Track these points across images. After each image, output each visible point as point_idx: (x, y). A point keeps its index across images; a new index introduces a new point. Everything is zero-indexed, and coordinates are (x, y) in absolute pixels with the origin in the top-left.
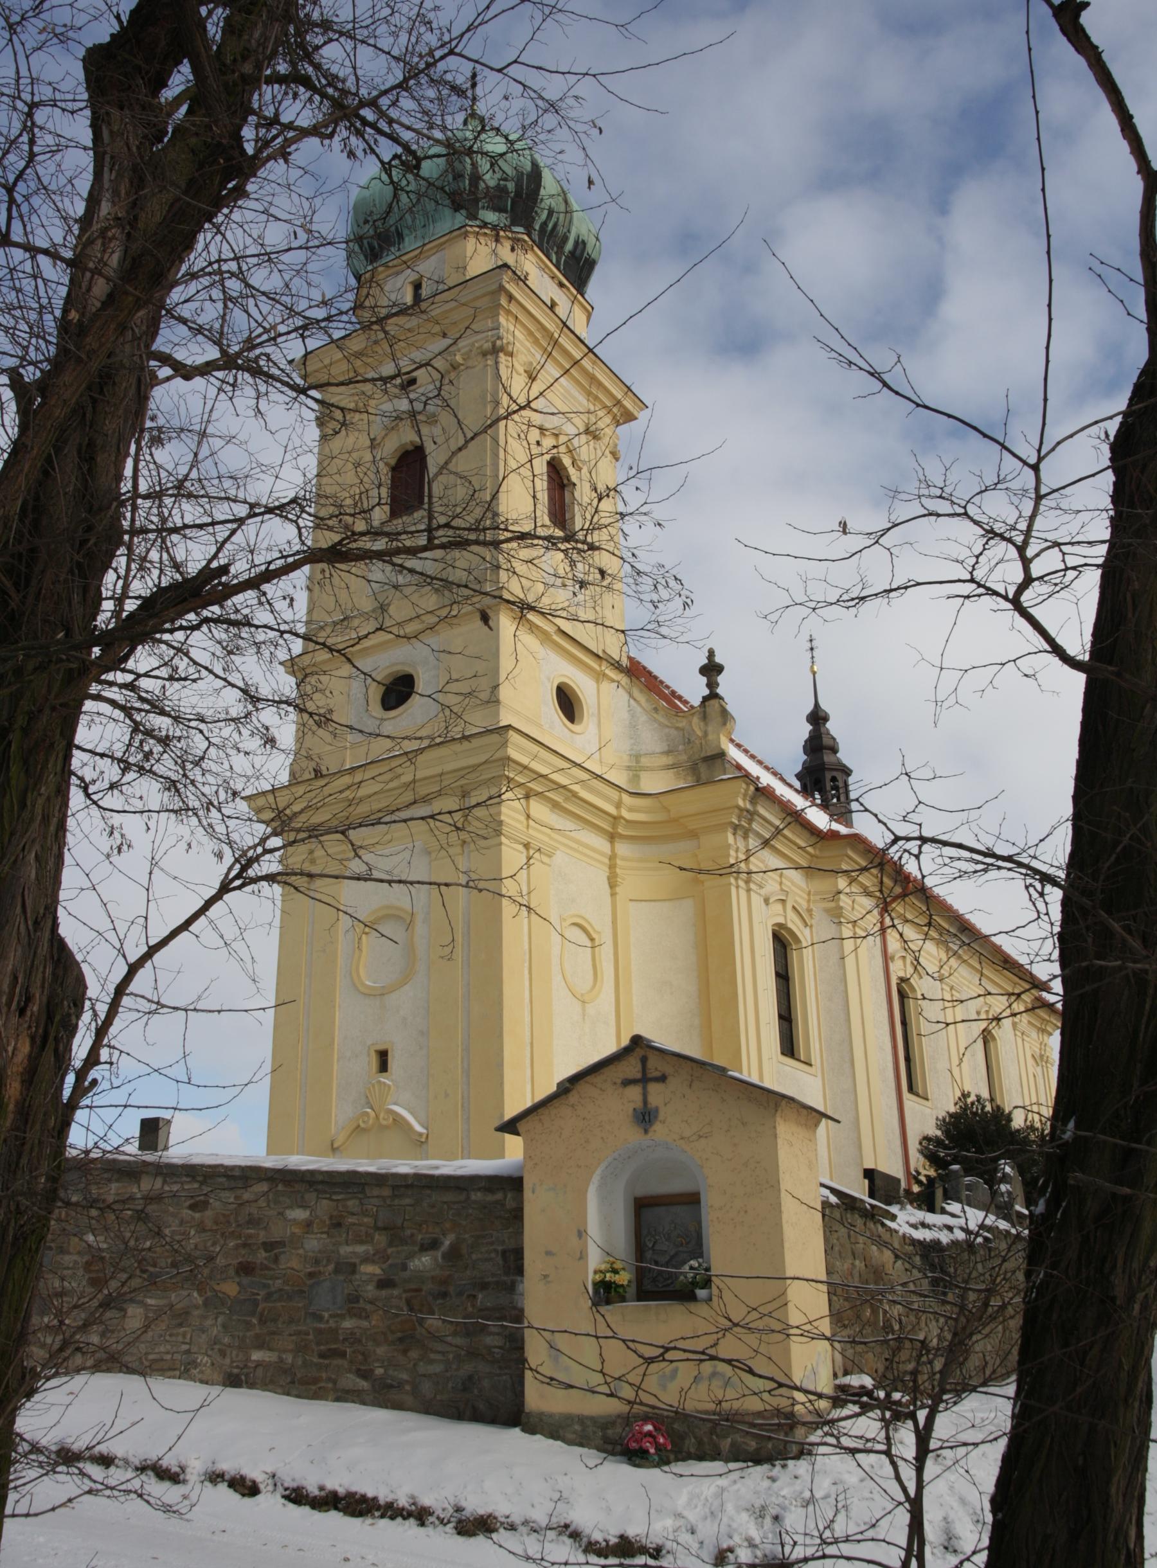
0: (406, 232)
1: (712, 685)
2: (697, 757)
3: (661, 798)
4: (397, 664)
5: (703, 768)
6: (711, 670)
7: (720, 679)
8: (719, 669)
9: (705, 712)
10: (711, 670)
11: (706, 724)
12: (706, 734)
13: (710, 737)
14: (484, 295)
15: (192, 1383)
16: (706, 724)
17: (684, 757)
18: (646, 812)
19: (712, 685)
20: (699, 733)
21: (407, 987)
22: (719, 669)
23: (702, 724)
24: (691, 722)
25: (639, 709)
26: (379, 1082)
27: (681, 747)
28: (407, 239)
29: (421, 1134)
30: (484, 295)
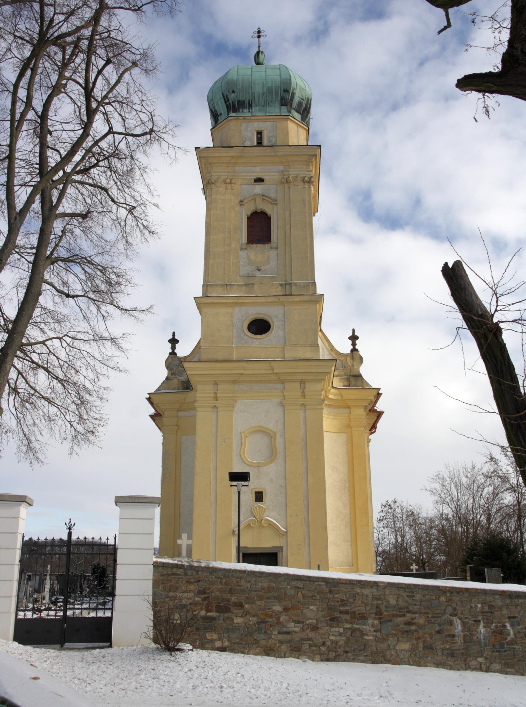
0: (253, 105)
1: (354, 344)
2: (348, 374)
3: (341, 390)
4: (261, 314)
5: (352, 379)
6: (354, 338)
7: (357, 342)
8: (357, 338)
9: (353, 356)
10: (354, 338)
11: (353, 361)
12: (353, 365)
13: (355, 367)
14: (306, 155)
15: (482, 673)
16: (353, 361)
17: (343, 373)
18: (334, 395)
19: (354, 344)
20: (350, 364)
21: (272, 465)
22: (357, 338)
23: (351, 361)
24: (346, 359)
25: (325, 348)
26: (260, 506)
27: (341, 368)
28: (253, 108)
29: (284, 531)
30: (306, 155)
